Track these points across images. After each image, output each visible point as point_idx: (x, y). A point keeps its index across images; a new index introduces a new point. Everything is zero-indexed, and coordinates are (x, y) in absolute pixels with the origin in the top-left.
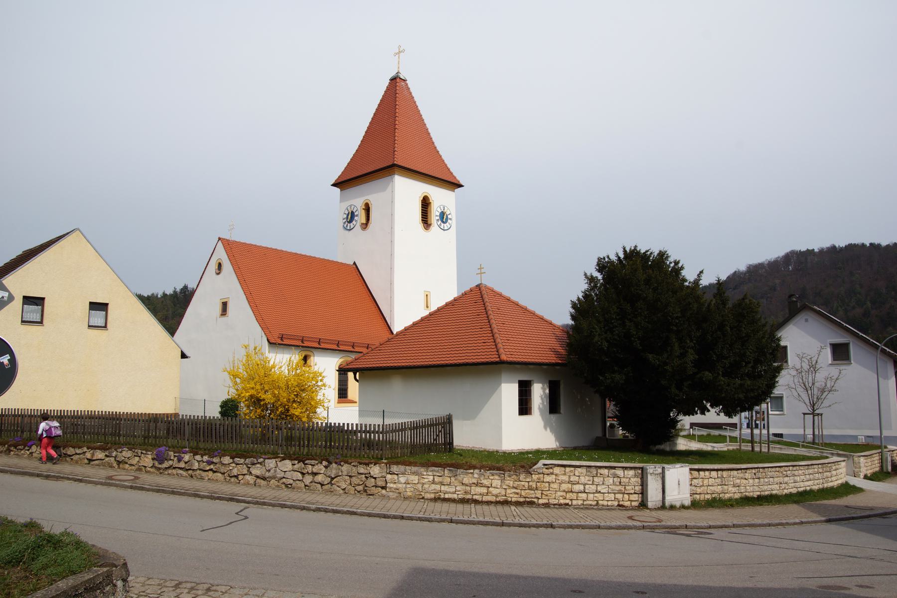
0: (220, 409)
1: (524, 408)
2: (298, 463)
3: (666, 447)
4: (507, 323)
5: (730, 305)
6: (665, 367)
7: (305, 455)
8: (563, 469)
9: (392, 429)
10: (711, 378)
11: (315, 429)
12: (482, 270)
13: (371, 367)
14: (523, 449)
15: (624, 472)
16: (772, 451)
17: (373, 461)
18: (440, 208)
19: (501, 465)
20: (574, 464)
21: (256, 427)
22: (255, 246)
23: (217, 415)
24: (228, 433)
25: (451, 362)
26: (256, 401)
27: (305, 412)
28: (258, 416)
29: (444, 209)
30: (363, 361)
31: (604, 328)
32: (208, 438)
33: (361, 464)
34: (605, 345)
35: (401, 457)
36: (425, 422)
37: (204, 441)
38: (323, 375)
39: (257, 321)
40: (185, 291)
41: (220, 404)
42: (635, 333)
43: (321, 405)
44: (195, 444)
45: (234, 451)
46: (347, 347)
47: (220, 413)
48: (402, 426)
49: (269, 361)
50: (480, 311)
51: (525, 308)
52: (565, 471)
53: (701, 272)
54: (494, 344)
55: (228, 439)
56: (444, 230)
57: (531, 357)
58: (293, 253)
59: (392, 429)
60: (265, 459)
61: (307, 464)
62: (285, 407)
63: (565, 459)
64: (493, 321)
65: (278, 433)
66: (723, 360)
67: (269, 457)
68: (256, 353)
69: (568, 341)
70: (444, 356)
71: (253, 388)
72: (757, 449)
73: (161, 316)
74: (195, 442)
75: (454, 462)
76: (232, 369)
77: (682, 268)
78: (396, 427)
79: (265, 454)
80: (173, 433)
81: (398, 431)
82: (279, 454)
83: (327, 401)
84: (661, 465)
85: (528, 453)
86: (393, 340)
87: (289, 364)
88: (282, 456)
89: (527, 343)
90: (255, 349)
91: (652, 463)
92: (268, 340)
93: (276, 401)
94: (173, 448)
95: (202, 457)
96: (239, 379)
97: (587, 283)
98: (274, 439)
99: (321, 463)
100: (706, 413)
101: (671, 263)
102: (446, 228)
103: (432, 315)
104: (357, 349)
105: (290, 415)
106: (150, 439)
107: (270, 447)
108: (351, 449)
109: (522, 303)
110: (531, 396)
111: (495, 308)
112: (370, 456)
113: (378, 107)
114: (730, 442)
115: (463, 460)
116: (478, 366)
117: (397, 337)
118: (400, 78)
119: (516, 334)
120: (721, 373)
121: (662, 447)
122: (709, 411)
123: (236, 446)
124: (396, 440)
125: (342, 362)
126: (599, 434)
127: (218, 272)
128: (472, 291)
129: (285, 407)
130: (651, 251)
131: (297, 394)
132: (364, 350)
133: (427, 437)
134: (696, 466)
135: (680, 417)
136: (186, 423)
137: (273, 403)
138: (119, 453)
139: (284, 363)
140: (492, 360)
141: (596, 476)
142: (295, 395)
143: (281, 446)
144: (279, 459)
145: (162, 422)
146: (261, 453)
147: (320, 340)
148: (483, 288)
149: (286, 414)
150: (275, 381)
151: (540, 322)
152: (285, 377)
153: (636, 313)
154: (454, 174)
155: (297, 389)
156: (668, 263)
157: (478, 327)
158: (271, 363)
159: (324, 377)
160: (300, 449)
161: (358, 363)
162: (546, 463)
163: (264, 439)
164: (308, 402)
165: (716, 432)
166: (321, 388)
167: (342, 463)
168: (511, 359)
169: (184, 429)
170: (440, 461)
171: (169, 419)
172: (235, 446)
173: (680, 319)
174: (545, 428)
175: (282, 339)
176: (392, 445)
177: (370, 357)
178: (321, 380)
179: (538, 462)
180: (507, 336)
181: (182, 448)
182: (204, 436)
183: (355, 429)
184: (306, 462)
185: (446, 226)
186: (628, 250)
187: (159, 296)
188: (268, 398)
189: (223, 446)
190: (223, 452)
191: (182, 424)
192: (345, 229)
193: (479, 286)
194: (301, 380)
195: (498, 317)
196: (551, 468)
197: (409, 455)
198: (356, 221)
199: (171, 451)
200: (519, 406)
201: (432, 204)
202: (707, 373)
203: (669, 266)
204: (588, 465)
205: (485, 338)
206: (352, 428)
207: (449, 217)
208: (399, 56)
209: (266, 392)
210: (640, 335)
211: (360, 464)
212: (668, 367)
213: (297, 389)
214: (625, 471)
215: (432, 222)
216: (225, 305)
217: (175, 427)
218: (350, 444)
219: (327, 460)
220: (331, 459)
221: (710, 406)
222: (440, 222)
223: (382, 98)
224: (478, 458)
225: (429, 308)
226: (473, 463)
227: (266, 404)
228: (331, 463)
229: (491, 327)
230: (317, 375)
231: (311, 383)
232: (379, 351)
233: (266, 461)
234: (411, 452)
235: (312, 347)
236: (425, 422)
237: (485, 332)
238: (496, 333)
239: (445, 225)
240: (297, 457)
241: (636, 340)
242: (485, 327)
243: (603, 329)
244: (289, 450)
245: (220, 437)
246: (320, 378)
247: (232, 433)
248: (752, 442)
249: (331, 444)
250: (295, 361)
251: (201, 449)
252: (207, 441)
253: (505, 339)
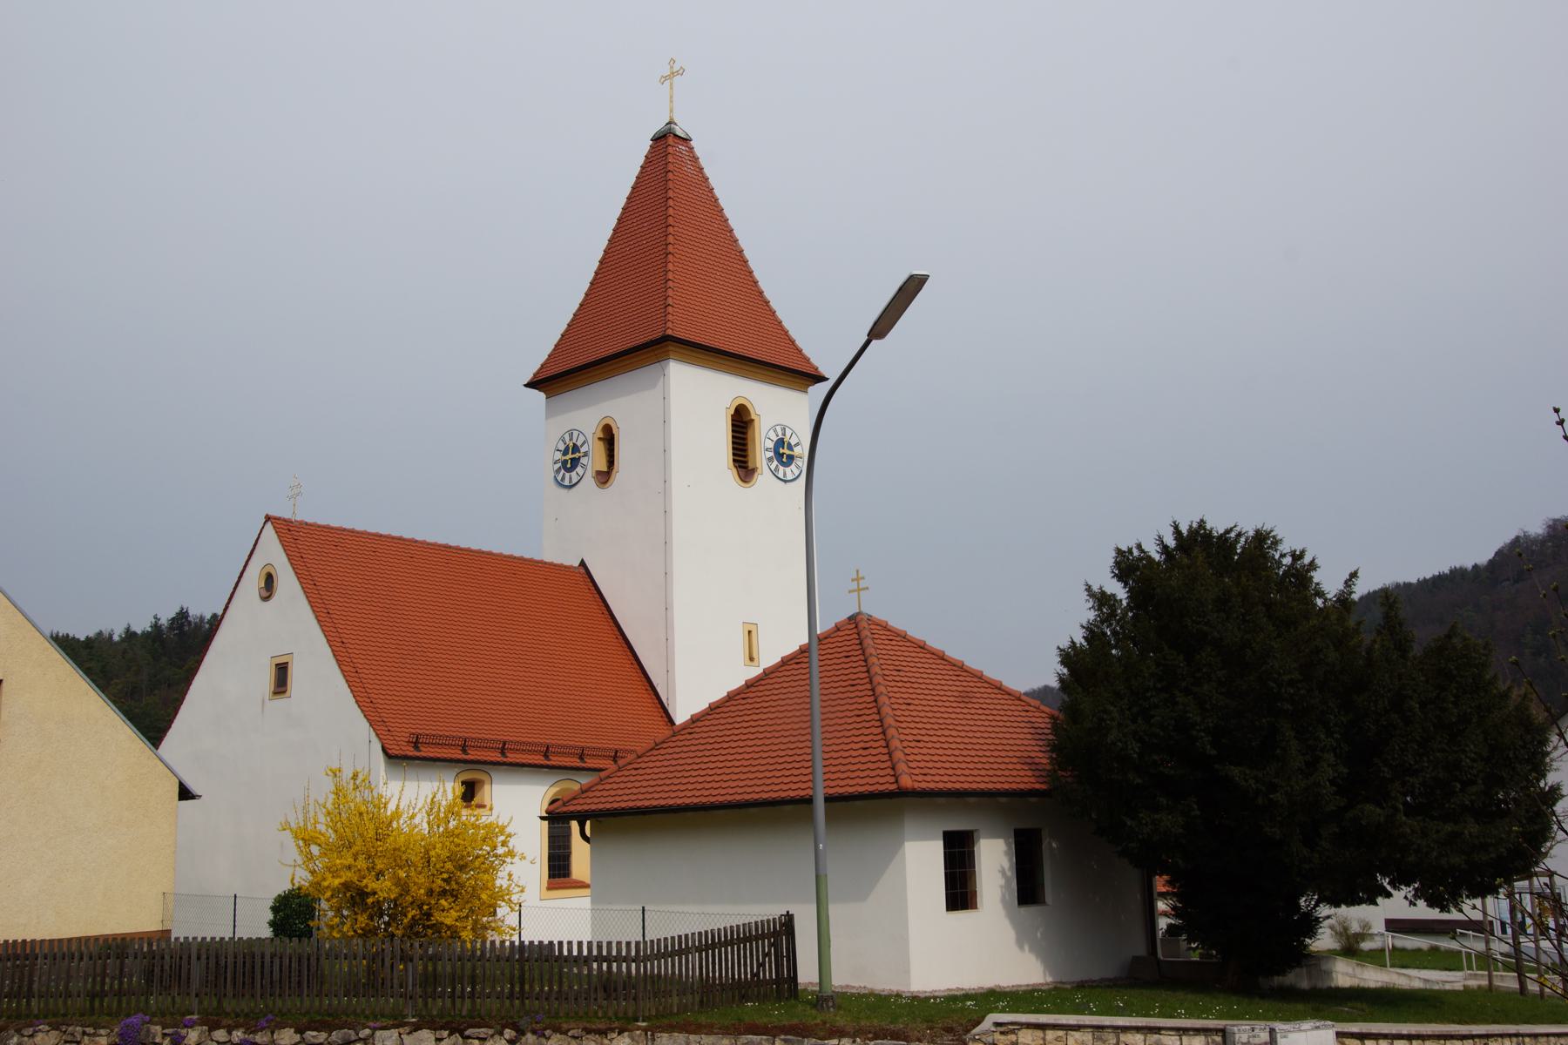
0: (270, 916)
1: (960, 894)
2: (450, 1035)
3: (1299, 979)
4: (916, 702)
5: (1416, 650)
6: (1271, 796)
7: (464, 1017)
8: (1039, 1033)
9: (659, 950)
10: (1382, 819)
11: (488, 955)
12: (861, 582)
13: (616, 809)
14: (958, 989)
15: (1181, 1039)
16: (1498, 984)
17: (616, 1024)
18: (775, 431)
19: (902, 1026)
20: (1064, 1022)
21: (355, 959)
22: (352, 531)
23: (267, 933)
24: (290, 972)
25: (792, 794)
26: (356, 897)
27: (467, 917)
28: (360, 931)
29: (784, 434)
30: (598, 794)
31: (1129, 709)
32: (243, 987)
33: (588, 1031)
34: (1132, 749)
35: (677, 1014)
36: (732, 932)
37: (234, 995)
38: (508, 830)
39: (359, 706)
40: (182, 625)
41: (270, 903)
42: (1198, 719)
43: (503, 900)
44: (215, 1003)
45: (304, 1015)
46: (566, 759)
47: (272, 924)
48: (680, 943)
49: (386, 804)
50: (856, 676)
51: (960, 665)
52: (1044, 1039)
53: (1354, 575)
54: (886, 751)
55: (290, 988)
56: (785, 481)
57: (971, 779)
58: (440, 545)
59: (659, 950)
60: (374, 1029)
61: (469, 1037)
62: (420, 907)
63: (1047, 1012)
64: (883, 699)
65: (406, 968)
66: (1408, 778)
67: (385, 1024)
68: (356, 788)
69: (1051, 737)
70: (777, 781)
71: (349, 867)
72: (1533, 987)
73: (120, 687)
74: (214, 998)
75: (795, 1021)
76: (302, 824)
77: (1313, 566)
78: (666, 947)
79: (375, 1018)
80: (161, 982)
81: (672, 955)
82: (405, 1016)
83: (517, 889)
84: (1269, 1023)
85: (967, 996)
86: (665, 745)
87: (431, 809)
88: (414, 1020)
89: (992, 747)
90: (355, 777)
91: (1249, 1019)
92: (384, 749)
93: (401, 895)
94: (162, 1016)
95: (230, 1033)
96: (318, 848)
97: (1093, 607)
98: (395, 981)
99: (501, 1034)
100: (1380, 900)
101: (1283, 556)
102: (789, 477)
103: (752, 685)
104: (590, 763)
105: (434, 925)
106: (106, 1000)
107: (387, 1001)
108: (566, 999)
109: (953, 653)
110: (974, 867)
111: (891, 667)
112: (611, 1013)
113: (627, 203)
114: (1478, 969)
115: (815, 1018)
116: (851, 803)
117: (674, 739)
118: (676, 136)
119: (936, 727)
120: (1401, 807)
121: (1277, 980)
122: (1389, 895)
123: (308, 1003)
124: (673, 972)
125: (555, 794)
126: (1141, 950)
127: (265, 594)
128: (839, 630)
129: (420, 907)
130: (1238, 529)
131: (450, 877)
132: (608, 764)
133: (740, 965)
134: (1355, 1028)
135: (1324, 910)
136: (194, 957)
137: (395, 900)
138: (26, 1039)
139: (420, 805)
140: (881, 788)
141: (1094, 1038)
142: (444, 880)
143: (411, 998)
144: (407, 1029)
145: (136, 958)
146: (367, 1017)
147: (504, 744)
148: (864, 624)
149: (424, 924)
150: (399, 850)
151: (993, 696)
152: (422, 840)
153: (1198, 675)
154: (806, 352)
155: (449, 866)
156: (1277, 557)
157: (852, 713)
158: (391, 807)
159: (510, 836)
160: (454, 1003)
161: (589, 801)
162: (999, 1021)
163: (373, 983)
164: (475, 895)
165: (1445, 944)
166: (504, 862)
167: (547, 1033)
168: (924, 785)
169: (189, 969)
170: (765, 1020)
171: (154, 948)
172: (307, 1003)
173: (1299, 685)
174: (1021, 947)
175: (416, 745)
176: (657, 986)
177: (615, 786)
178: (504, 844)
179: (983, 1018)
180: (915, 732)
181: (184, 1015)
182: (235, 984)
183: (585, 953)
184: (467, 1033)
186: (1184, 529)
187: (116, 638)
188: (384, 888)
189: (279, 1003)
190: (278, 1019)
191: (185, 957)
192: (560, 484)
193: (853, 619)
194: (458, 845)
195: (896, 689)
196: (1013, 1032)
197: (696, 1008)
198: (584, 466)
199: (157, 1025)
200: (947, 889)
201: (756, 423)
202: (1369, 807)
203: (1279, 563)
204: (1095, 1023)
205: (866, 739)
206: (570, 950)
208: (671, 84)
209: (380, 874)
210: (1211, 725)
211: (587, 1034)
212: (1278, 794)
213: (449, 866)
214: (1184, 1037)
215: (758, 465)
216: (282, 673)
217: (167, 967)
218: (565, 988)
219: (515, 1027)
220: (523, 1023)
221: (1389, 883)
222: (775, 463)
223: (636, 183)
224: (850, 1011)
225: (756, 660)
226: (838, 1024)
227: (378, 902)
228: (523, 1033)
229: (879, 713)
230: (493, 833)
231: (481, 849)
232: (634, 772)
233: (378, 1033)
234: (701, 1002)
235: (485, 763)
236: (732, 932)
237: (867, 725)
238: (890, 726)
239: (788, 470)
240: (447, 1023)
241: (1203, 734)
242: (868, 712)
243: (1127, 712)
244: (430, 1005)
245: (271, 983)
246: (502, 838)
247: (299, 971)
248: (1519, 970)
249: (522, 988)
250: (444, 803)
251: (227, 1014)
252: (243, 995)
253: (910, 737)
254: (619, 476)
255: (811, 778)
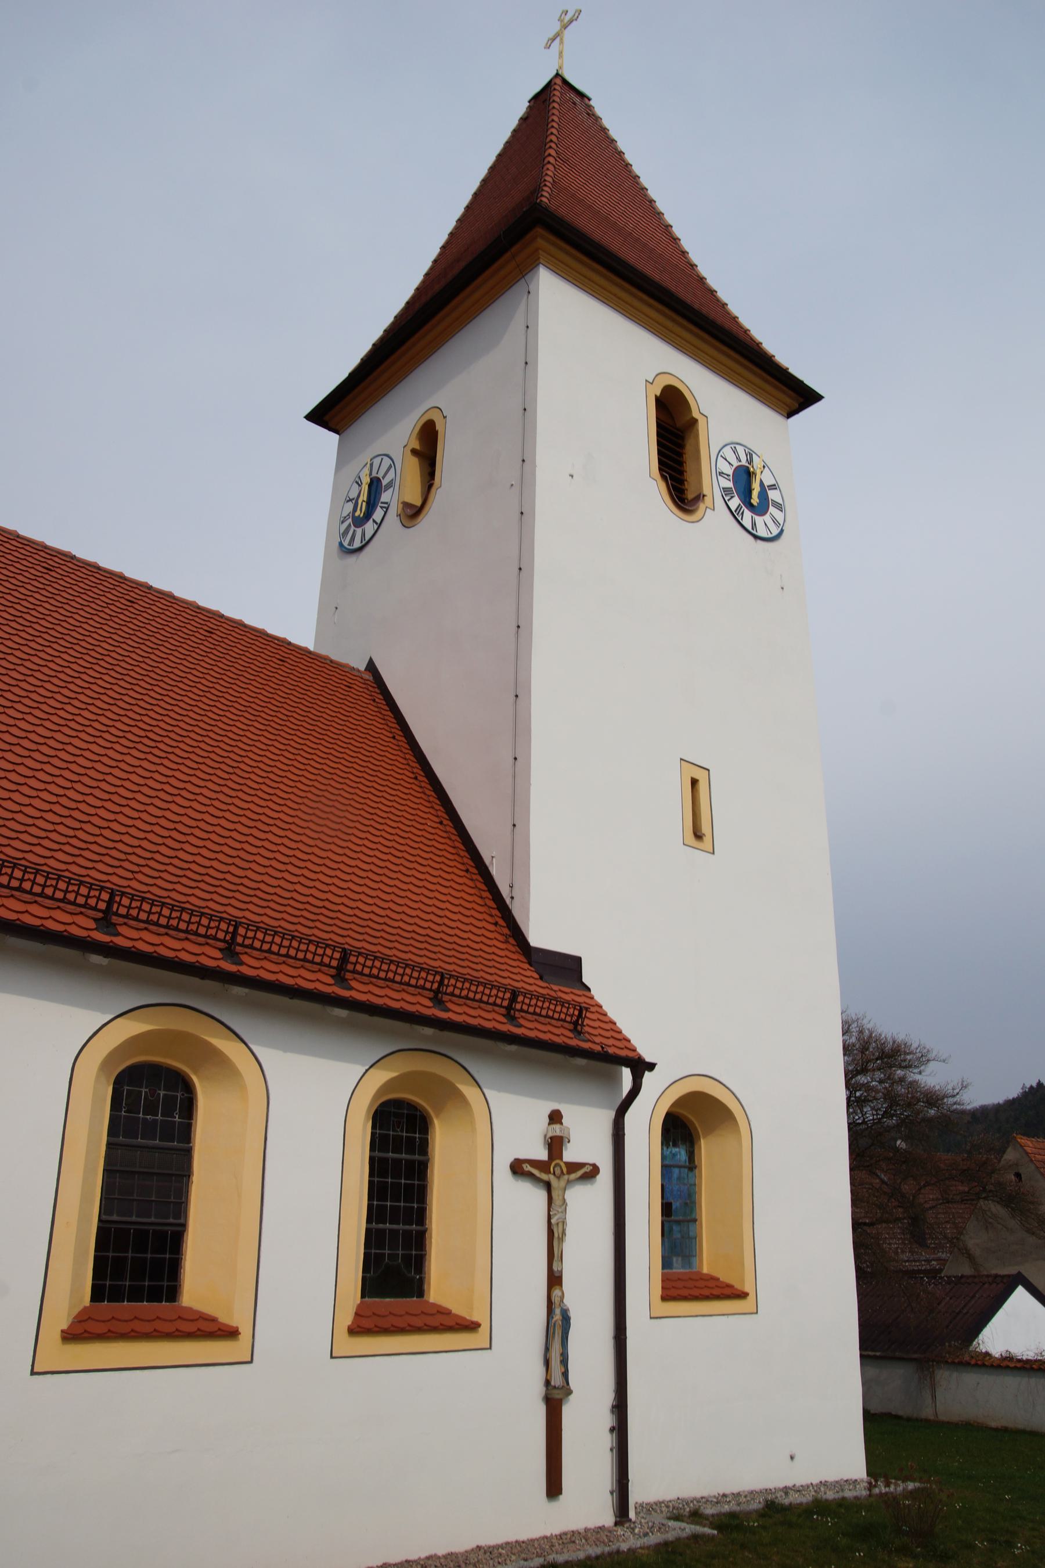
56: (756, 537)
102: (762, 532)
185: (764, 525)
207: (773, 495)
215: (706, 490)
225: (707, 839)
254: (352, 559)
255: (76, 890)
